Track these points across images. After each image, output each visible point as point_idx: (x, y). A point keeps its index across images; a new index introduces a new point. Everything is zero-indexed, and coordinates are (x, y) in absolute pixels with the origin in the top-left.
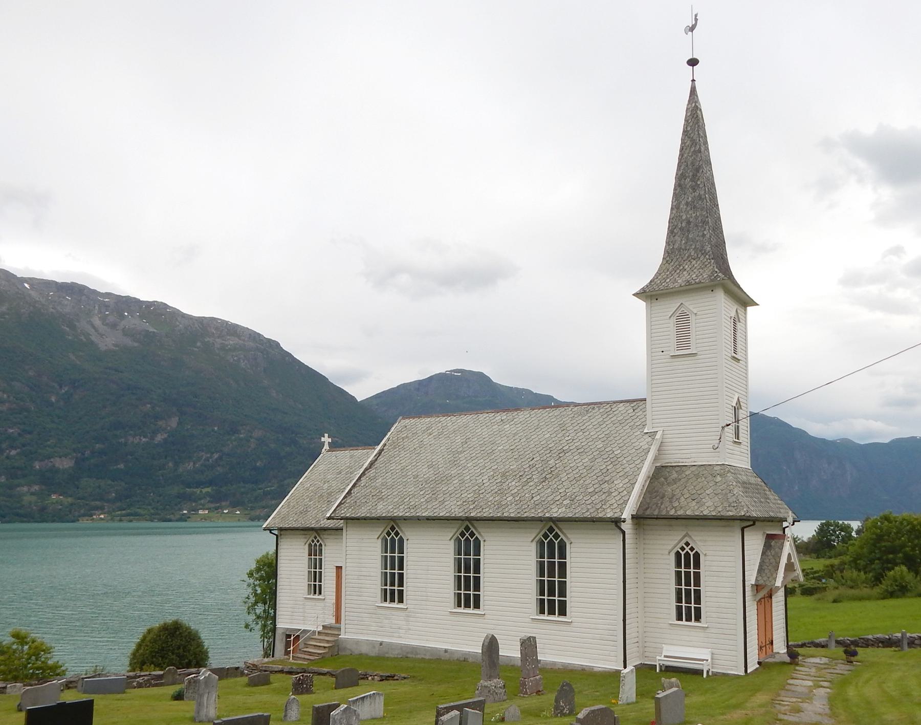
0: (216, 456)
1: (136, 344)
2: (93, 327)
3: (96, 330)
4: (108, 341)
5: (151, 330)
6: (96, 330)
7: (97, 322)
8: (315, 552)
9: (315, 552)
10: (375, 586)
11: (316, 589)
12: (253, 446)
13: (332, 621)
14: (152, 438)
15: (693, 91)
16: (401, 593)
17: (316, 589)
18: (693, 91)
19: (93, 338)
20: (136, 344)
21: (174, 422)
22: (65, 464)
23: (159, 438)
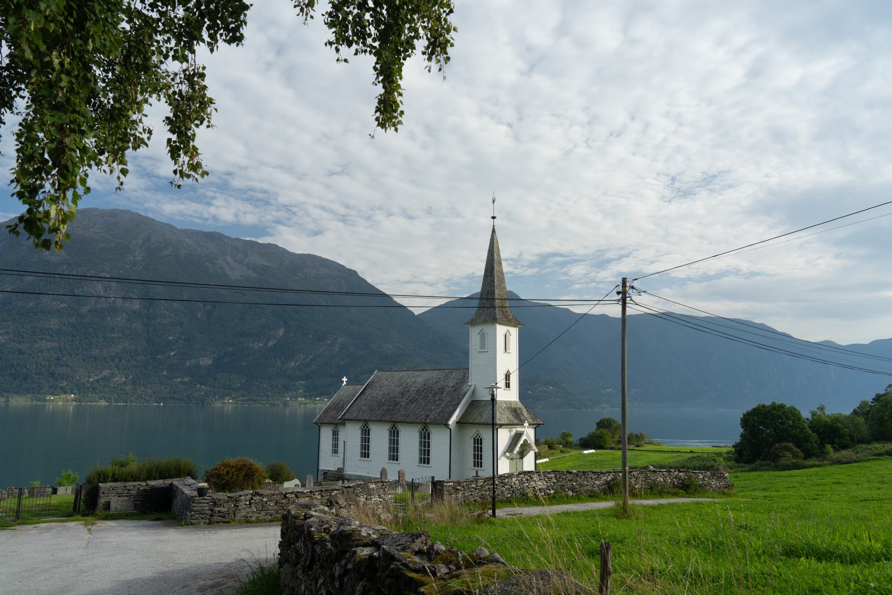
0: (311, 357)
1: (256, 275)
2: (227, 262)
3: (229, 265)
4: (236, 274)
5: (266, 264)
6: (229, 265)
7: (230, 259)
8: (335, 434)
9: (335, 434)
10: (416, 456)
11: (335, 451)
12: (337, 350)
13: (341, 466)
14: (265, 344)
15: (494, 231)
16: (428, 459)
17: (335, 451)
18: (494, 231)
19: (226, 271)
20: (256, 275)
21: (281, 332)
22: (206, 361)
23: (271, 344)
